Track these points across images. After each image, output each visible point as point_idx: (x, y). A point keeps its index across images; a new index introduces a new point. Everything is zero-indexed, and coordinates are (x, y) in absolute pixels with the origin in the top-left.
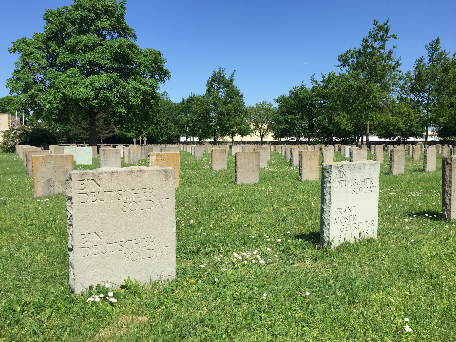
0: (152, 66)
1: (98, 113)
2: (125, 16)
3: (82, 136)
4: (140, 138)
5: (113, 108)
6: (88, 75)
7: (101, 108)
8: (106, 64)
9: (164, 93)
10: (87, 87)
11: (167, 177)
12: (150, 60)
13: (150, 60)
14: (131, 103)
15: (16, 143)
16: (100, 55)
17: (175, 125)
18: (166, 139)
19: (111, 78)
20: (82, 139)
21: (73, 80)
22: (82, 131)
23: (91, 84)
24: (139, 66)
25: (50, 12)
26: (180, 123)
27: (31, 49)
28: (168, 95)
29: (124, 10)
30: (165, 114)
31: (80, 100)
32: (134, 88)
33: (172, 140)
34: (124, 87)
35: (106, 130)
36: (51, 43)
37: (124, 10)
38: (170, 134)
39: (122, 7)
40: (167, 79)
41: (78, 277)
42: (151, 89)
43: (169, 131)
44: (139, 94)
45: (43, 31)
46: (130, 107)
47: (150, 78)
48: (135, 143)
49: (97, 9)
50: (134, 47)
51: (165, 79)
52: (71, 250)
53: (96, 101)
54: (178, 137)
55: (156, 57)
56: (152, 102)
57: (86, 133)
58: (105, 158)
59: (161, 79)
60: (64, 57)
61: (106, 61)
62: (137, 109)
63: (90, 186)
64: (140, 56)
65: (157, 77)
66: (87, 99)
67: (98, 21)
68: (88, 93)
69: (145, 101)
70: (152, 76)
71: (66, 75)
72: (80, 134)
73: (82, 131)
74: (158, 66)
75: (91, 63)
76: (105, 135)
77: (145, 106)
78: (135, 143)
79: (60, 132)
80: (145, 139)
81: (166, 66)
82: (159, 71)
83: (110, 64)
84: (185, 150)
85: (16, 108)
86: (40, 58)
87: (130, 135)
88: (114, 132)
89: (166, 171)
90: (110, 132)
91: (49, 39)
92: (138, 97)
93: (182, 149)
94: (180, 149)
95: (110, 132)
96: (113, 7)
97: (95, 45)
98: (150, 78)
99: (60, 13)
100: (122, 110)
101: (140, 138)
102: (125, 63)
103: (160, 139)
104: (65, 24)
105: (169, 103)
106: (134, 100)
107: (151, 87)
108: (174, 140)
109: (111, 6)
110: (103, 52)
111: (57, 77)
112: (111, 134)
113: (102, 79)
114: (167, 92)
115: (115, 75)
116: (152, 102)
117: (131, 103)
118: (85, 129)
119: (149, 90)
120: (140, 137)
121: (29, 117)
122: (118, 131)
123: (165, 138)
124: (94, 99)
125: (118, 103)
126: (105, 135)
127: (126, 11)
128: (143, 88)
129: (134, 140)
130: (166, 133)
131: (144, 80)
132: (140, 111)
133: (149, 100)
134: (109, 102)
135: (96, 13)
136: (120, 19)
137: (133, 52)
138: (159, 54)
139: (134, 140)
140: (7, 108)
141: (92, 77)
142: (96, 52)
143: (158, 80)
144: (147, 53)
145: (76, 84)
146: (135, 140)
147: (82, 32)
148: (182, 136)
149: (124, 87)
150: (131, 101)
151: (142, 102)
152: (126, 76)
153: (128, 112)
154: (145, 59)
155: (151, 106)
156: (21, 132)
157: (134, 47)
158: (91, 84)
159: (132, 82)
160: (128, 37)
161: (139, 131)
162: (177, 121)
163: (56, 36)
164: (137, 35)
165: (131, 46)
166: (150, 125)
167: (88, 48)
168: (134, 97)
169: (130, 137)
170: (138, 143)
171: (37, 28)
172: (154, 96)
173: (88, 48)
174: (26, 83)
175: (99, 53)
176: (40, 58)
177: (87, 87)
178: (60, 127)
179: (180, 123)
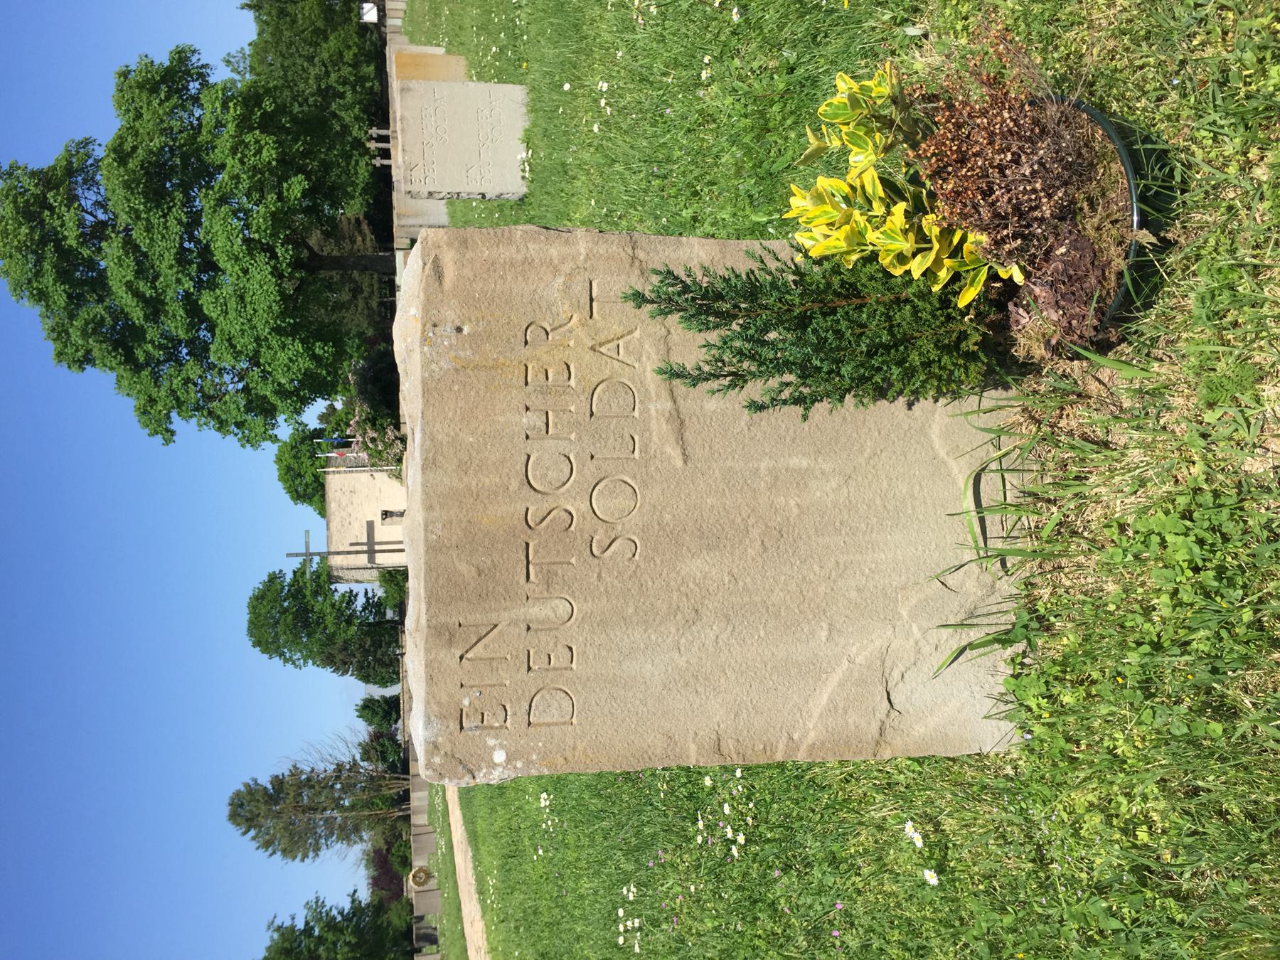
0: (167, 98)
1: (310, 249)
2: (35, 165)
3: (374, 304)
4: (372, 145)
5: (294, 211)
6: (214, 267)
7: (297, 241)
8: (180, 222)
9: (228, 62)
10: (245, 271)
11: (409, 90)
12: (149, 103)
13: (149, 103)
14: (274, 163)
15: (396, 438)
16: (157, 237)
17: (326, 39)
18: (372, 68)
19: (215, 211)
20: (381, 304)
21: (232, 304)
22: (361, 303)
23: (237, 259)
24: (167, 132)
25: (60, 354)
26: (320, 24)
27: (163, 393)
28: (233, 53)
29: (19, 168)
30: (294, 64)
31: (282, 293)
32: (234, 151)
33: (373, 45)
34: (236, 178)
35: (353, 242)
36: (140, 355)
37: (19, 168)
38: (355, 55)
39: (10, 174)
40: (197, 56)
41: (511, 189)
42: (231, 104)
43: (349, 56)
44: (248, 138)
45: (112, 376)
46: (287, 165)
47: (201, 106)
48: (386, 162)
49: (32, 239)
50: (121, 145)
51: (200, 64)
52: (484, 196)
53: (279, 251)
54: (364, 28)
55: (141, 86)
56: (268, 105)
57: (366, 294)
58: (416, 215)
59: (202, 76)
60: (176, 323)
61: (172, 222)
62: (291, 147)
63: (417, 174)
64: (141, 131)
65: (194, 86)
66: (277, 273)
67: (65, 238)
68: (261, 271)
69: (268, 123)
70: (196, 100)
71: (222, 318)
72: (369, 308)
73: (361, 303)
74: (164, 80)
75: (182, 258)
76: (368, 243)
77: (283, 129)
78: (386, 162)
79: (364, 359)
80: (374, 132)
81: (162, 58)
82: (175, 78)
83: (178, 213)
84: (401, 14)
85: (310, 458)
86: (184, 375)
87: (363, 174)
88: (357, 220)
89: (402, 90)
90: (360, 232)
91: (130, 359)
92: (257, 142)
93: (399, 22)
94: (397, 31)
95: (360, 232)
96: (15, 197)
97: (130, 245)
98: (201, 106)
99: (60, 333)
100: (296, 186)
101: (372, 145)
102: (169, 173)
103: (372, 88)
104: (87, 323)
105: (260, 49)
106: (265, 153)
107: (225, 106)
108: (372, 43)
109: (15, 202)
110: (149, 229)
111: (229, 340)
112: (365, 227)
113: (221, 234)
114: (224, 55)
115: (203, 201)
116: (268, 105)
117: (274, 163)
118: (355, 297)
119: (234, 111)
120: (368, 145)
121: (329, 429)
122: (353, 209)
123: (370, 69)
124: (274, 256)
125: (280, 197)
126: (368, 243)
127: (21, 164)
128: (231, 128)
129: (378, 165)
130: (355, 65)
131: (208, 120)
132: (296, 140)
133: (265, 114)
134: (279, 219)
135: (43, 242)
136: (47, 179)
137: (134, 148)
138: (125, 74)
139: (378, 165)
140: (309, 478)
141: (221, 259)
142: (151, 246)
143: (205, 84)
144: (128, 110)
145: (242, 298)
146: (378, 162)
147: (99, 284)
148: (360, 16)
149: (236, 178)
150: (269, 163)
151: (269, 134)
152: (207, 173)
153: (301, 170)
154: (146, 116)
155: (281, 109)
156: (368, 427)
157: (121, 145)
158: (237, 259)
159: (216, 157)
160: (90, 161)
161: (353, 148)
162: (317, 31)
163: (122, 341)
164: (79, 138)
165: (121, 154)
166: (334, 115)
167: (144, 266)
168: (259, 152)
169: (372, 175)
170: (386, 154)
171: (104, 393)
172: (251, 99)
173: (144, 266)
174: (248, 409)
175: (152, 239)
176: (184, 375)
177: (245, 271)
178: (351, 357)
179: (320, 24)
